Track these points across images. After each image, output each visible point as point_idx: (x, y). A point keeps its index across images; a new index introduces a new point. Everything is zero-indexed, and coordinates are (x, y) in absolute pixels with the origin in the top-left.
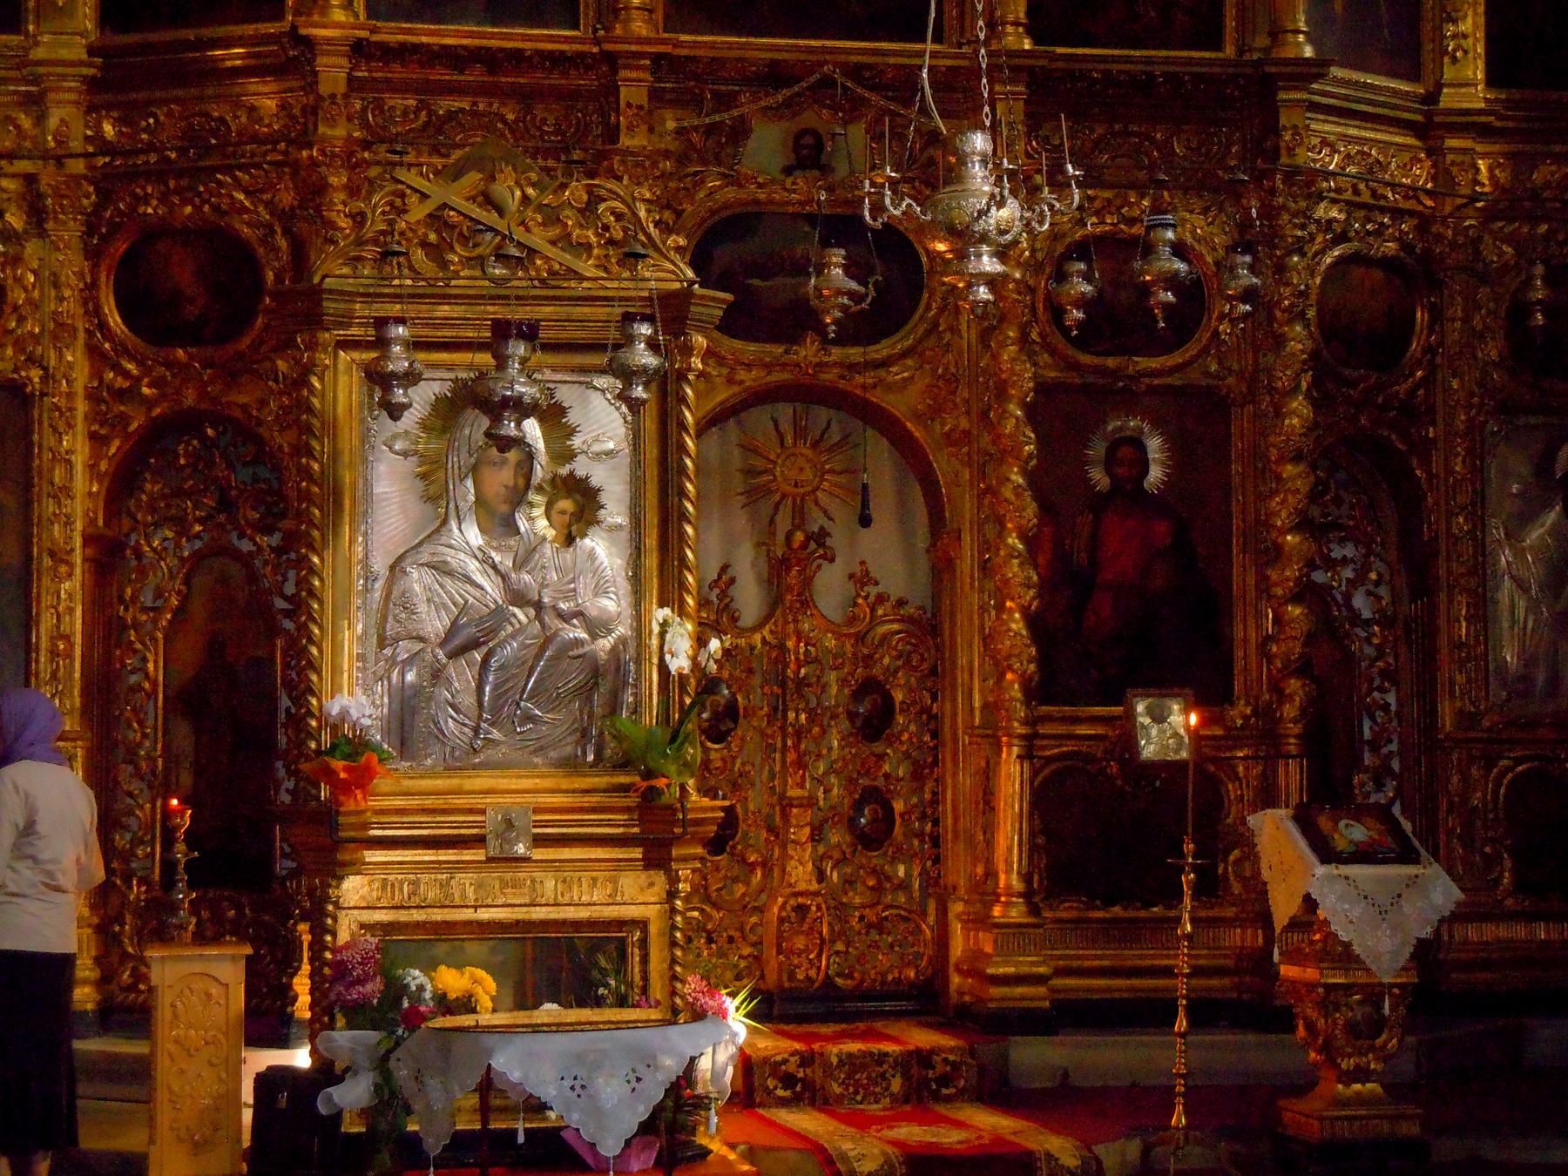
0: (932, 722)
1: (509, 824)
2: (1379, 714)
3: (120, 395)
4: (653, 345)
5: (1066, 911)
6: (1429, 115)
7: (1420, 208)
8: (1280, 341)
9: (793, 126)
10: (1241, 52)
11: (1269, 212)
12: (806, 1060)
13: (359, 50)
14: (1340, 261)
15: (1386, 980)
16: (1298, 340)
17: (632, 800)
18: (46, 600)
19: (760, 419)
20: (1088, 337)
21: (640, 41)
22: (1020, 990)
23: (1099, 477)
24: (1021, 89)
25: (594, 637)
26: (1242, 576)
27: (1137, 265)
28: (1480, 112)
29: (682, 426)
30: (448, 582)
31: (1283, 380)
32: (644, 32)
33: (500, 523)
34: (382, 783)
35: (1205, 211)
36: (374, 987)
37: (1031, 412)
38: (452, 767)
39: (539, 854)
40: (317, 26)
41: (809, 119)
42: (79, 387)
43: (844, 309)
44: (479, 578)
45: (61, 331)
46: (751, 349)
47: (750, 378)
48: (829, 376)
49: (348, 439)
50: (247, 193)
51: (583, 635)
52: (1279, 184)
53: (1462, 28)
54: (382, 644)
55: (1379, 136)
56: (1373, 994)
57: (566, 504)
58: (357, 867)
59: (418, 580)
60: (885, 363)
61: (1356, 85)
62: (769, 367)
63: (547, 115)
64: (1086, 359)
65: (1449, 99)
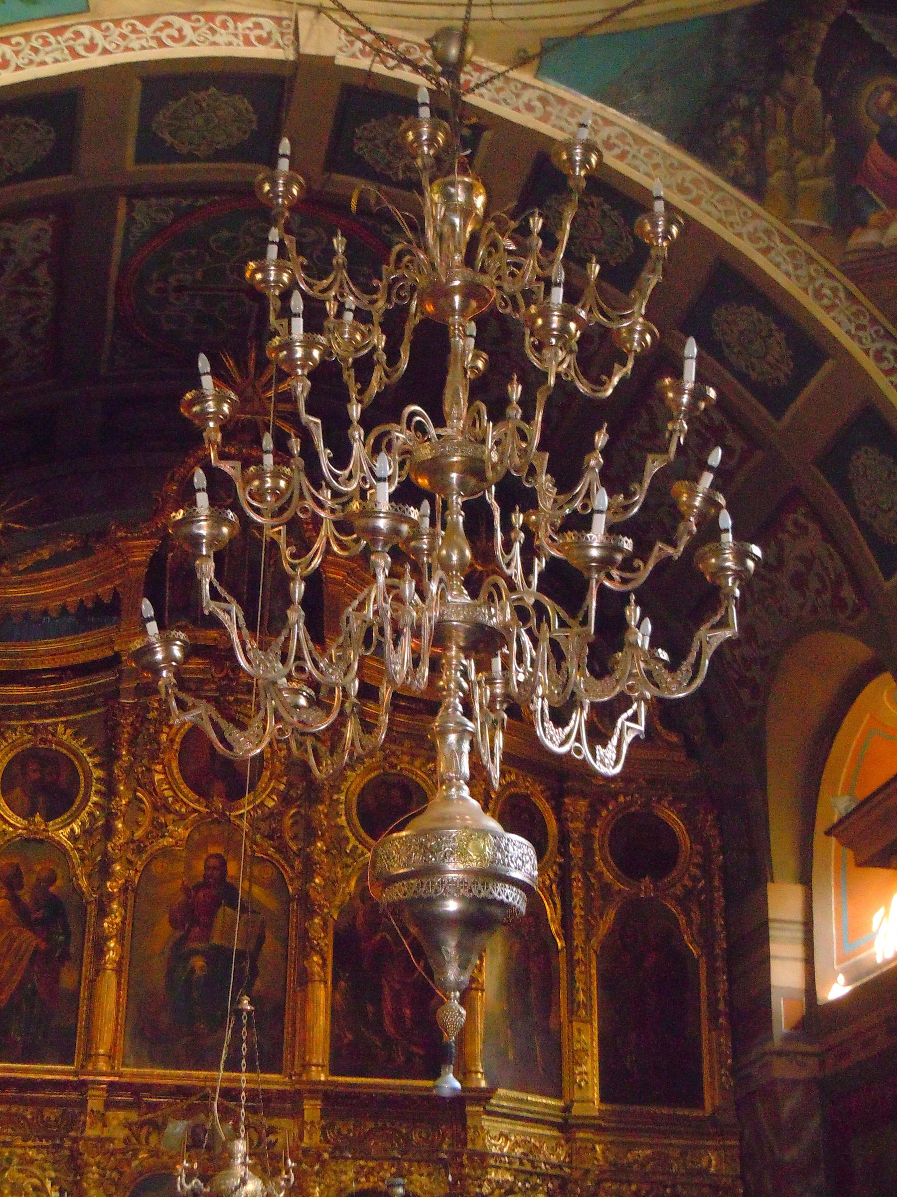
6: (566, 1120)
7: (562, 1173)
24: (319, 1102)
28: (594, 1118)
32: (104, 1069)
52: (466, 1162)
53: (584, 1068)
55: (536, 1131)
61: (520, 1101)
63: (52, 1114)
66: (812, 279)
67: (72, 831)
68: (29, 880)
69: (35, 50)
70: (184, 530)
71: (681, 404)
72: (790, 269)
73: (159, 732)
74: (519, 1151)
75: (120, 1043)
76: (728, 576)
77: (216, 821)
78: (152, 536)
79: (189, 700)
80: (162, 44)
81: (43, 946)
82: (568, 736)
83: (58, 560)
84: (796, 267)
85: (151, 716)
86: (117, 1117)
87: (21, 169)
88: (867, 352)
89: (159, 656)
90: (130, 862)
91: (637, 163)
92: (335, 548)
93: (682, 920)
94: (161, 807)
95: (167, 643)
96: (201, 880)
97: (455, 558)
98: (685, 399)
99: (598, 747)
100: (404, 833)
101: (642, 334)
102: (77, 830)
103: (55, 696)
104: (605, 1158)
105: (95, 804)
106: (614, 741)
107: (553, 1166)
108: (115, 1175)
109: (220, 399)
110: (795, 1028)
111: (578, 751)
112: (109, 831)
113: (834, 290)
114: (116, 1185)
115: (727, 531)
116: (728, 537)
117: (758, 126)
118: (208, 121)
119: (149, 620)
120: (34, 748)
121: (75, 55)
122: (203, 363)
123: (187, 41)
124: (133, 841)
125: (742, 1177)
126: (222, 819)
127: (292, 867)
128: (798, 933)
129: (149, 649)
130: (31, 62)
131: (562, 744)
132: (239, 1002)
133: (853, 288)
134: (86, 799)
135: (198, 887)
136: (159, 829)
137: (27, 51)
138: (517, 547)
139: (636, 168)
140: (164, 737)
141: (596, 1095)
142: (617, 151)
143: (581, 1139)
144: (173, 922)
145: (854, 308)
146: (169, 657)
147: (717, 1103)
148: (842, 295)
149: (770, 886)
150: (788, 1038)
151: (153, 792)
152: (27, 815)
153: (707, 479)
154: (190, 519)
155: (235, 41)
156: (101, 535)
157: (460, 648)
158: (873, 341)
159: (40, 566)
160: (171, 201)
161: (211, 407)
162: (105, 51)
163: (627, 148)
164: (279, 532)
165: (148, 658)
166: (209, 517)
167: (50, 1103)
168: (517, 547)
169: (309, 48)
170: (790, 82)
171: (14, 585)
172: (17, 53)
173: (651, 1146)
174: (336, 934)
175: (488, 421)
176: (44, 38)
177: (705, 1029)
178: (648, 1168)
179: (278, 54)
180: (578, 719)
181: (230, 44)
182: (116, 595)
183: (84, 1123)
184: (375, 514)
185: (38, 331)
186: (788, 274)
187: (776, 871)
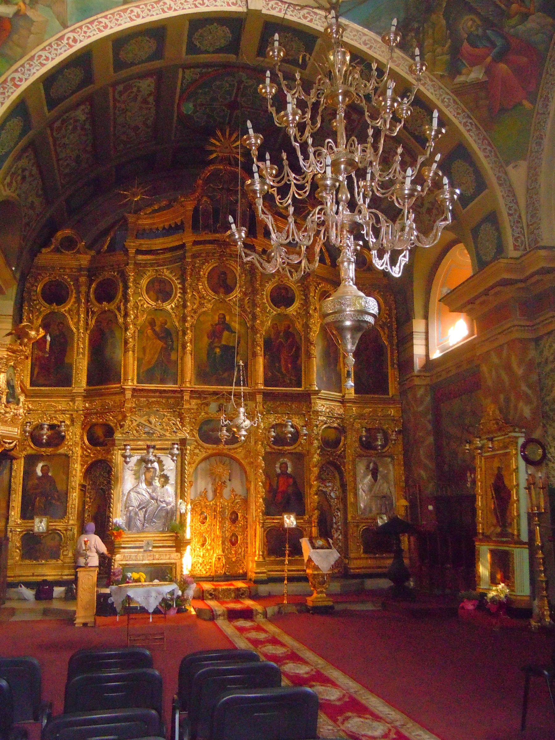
0: (245, 519)
1: (148, 543)
2: (337, 517)
3: (87, 456)
4: (178, 449)
5: (272, 558)
8: (312, 444)
9: (219, 403)
10: (305, 388)
11: (310, 419)
12: (215, 590)
13: (134, 390)
14: (325, 428)
15: (326, 573)
16: (316, 443)
17: (174, 538)
18: (71, 497)
19: (213, 459)
20: (275, 443)
21: (188, 387)
22: (261, 575)
23: (278, 471)
25: (167, 505)
26: (307, 489)
27: (284, 429)
29: (185, 464)
30: (139, 495)
31: (313, 451)
33: (149, 483)
34: (124, 536)
35: (299, 418)
36: (120, 577)
37: (264, 459)
38: (139, 532)
39: (155, 550)
40: (126, 386)
41: (222, 401)
42: (79, 455)
43: (226, 439)
44: (145, 494)
45: (76, 444)
46: (210, 446)
47: (210, 452)
48: (225, 451)
49: (120, 467)
50: (113, 417)
51: (165, 505)
54: (125, 508)
56: (323, 576)
57: (162, 480)
58: (119, 553)
59: (133, 494)
60: (236, 448)
62: (213, 449)
63: (171, 401)
64: (276, 447)
65: (347, 397)
66: (441, 95)
67: (172, 306)
68: (158, 323)
69: (149, 10)
70: (251, 188)
71: (432, 135)
72: (433, 91)
73: (199, 271)
74: (328, 410)
75: (193, 377)
76: (446, 202)
77: (221, 302)
78: (194, 200)
79: (248, 252)
80: (196, 6)
81: (165, 346)
82: (383, 263)
83: (160, 209)
84: (435, 91)
85: (197, 265)
86: (194, 402)
87: (144, 58)
88: (460, 123)
89: (237, 237)
90: (192, 316)
91: (376, 50)
92: (297, 196)
93: (382, 333)
94: (203, 297)
95: (239, 232)
96: (217, 322)
97: (344, 198)
98: (433, 133)
99: (393, 267)
100: (331, 298)
101: (407, 110)
102: (173, 306)
103: (163, 259)
104: (356, 412)
105: (179, 297)
106: (398, 264)
107: (339, 414)
108: (194, 420)
109: (256, 138)
110: (422, 368)
111: (387, 268)
112: (185, 306)
113: (449, 99)
114: (194, 423)
115: (446, 184)
116: (447, 187)
117: (421, 35)
118: (213, 37)
119: (232, 223)
120: (156, 277)
121: (164, 12)
122: (249, 124)
123: (206, 5)
124: (193, 309)
125: (402, 417)
126: (223, 301)
127: (248, 317)
128: (423, 336)
129: (233, 235)
130: (148, 15)
131: (382, 266)
132: (239, 362)
133: (455, 98)
134: (176, 294)
135: (216, 325)
136: (201, 305)
137: (146, 11)
138: (361, 194)
139: (375, 53)
140: (202, 273)
141: (353, 392)
142: (368, 46)
143: (349, 406)
144: (208, 337)
145: (456, 106)
146: (240, 237)
147: (394, 393)
148: (452, 101)
149: (414, 320)
150: (420, 371)
151: (199, 292)
152: (156, 300)
153: (435, 166)
154: (253, 184)
155: (224, 5)
156: (175, 200)
157: (347, 231)
158: (463, 118)
159: (155, 211)
160: (198, 70)
161: (253, 141)
162: (175, 10)
163: (372, 44)
164: (274, 190)
165: (233, 238)
166: (260, 183)
167: (171, 397)
168: (361, 194)
169: (251, 7)
170: (434, 17)
171: (146, 219)
172: (142, 11)
173: (371, 408)
174: (264, 339)
175: (358, 144)
176: (152, 5)
177: (389, 368)
178: (371, 415)
179: (240, 9)
180: (387, 257)
181: (222, 6)
182: (182, 223)
183: (183, 404)
184: (326, 179)
185: (149, 122)
186: (432, 93)
187: (416, 315)
